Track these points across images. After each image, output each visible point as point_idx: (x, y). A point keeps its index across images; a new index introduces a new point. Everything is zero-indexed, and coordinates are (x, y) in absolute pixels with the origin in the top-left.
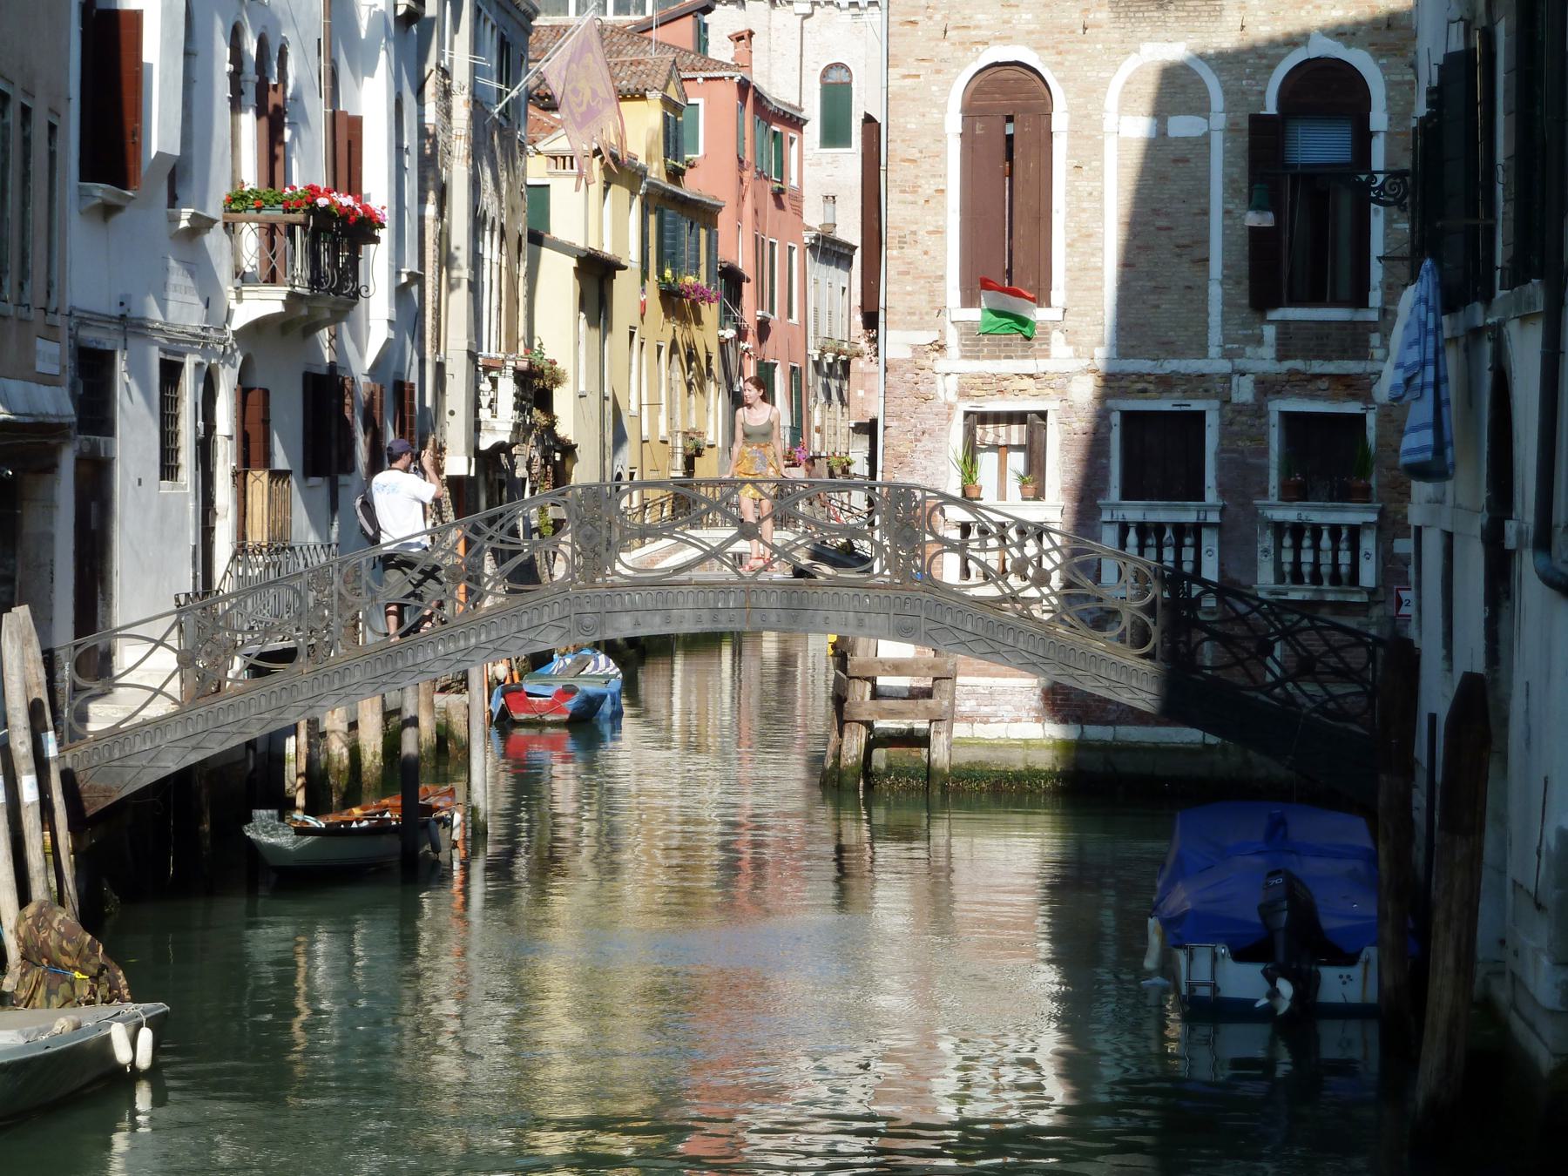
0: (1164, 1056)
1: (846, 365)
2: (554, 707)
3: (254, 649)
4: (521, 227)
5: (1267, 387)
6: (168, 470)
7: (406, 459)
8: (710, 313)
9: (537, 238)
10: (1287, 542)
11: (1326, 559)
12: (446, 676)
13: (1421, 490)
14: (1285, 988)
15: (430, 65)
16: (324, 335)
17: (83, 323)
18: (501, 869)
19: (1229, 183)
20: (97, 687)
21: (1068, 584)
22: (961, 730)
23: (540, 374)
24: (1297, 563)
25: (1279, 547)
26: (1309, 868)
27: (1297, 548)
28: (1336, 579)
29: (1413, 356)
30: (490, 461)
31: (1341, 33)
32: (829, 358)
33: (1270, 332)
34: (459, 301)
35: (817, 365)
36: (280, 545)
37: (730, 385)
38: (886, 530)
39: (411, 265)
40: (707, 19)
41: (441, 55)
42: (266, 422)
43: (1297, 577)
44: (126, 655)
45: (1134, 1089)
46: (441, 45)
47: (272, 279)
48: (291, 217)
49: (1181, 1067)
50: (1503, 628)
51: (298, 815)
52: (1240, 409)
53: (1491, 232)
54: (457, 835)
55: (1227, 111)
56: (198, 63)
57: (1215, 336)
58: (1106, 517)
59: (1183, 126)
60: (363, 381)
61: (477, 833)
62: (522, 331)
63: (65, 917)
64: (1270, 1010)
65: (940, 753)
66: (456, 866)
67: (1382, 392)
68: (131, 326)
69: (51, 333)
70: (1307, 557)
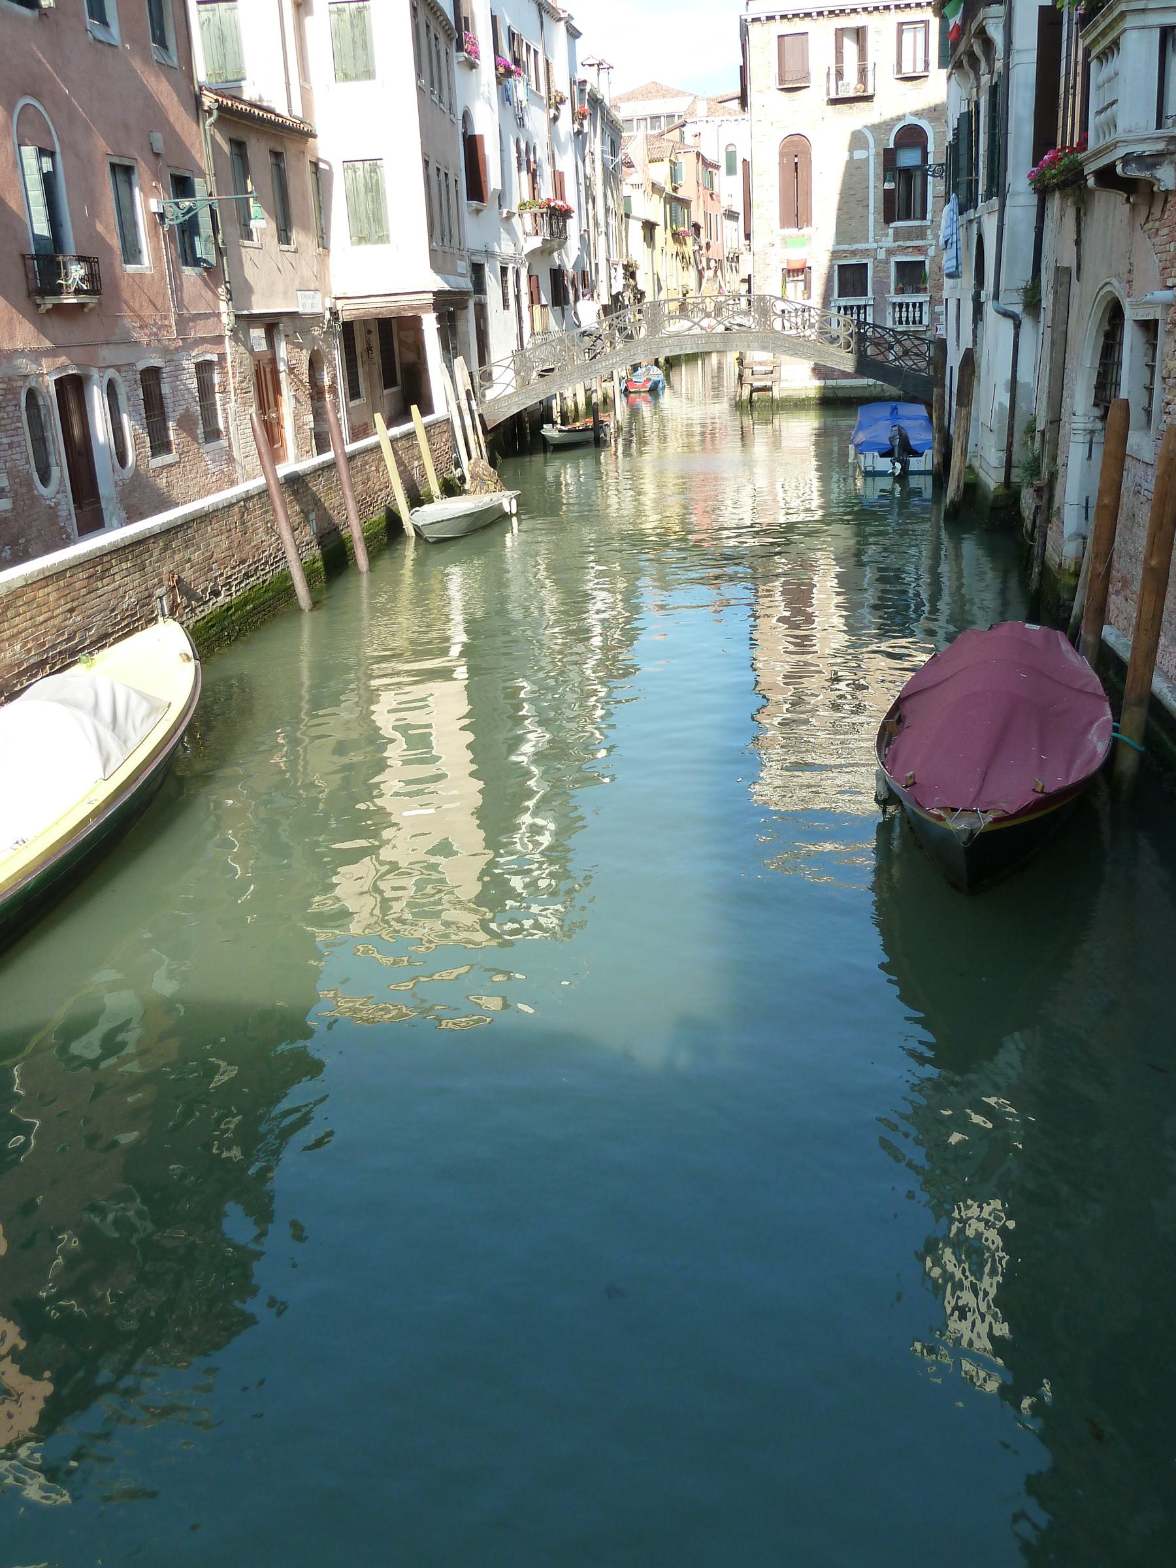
0: (855, 490)
1: (738, 257)
2: (644, 386)
3: (540, 369)
4: (622, 212)
5: (890, 252)
6: (506, 306)
7: (588, 296)
8: (689, 240)
9: (627, 216)
10: (897, 309)
11: (910, 315)
12: (606, 375)
13: (948, 283)
14: (898, 465)
15: (587, 151)
16: (556, 254)
17: (472, 254)
18: (628, 444)
19: (876, 175)
20: (488, 384)
21: (820, 328)
22: (783, 385)
23: (631, 266)
24: (901, 317)
25: (894, 311)
26: (905, 424)
27: (901, 311)
28: (914, 322)
29: (949, 231)
30: (616, 298)
31: (917, 114)
32: (731, 255)
33: (891, 231)
34: (602, 238)
35: (727, 258)
36: (546, 332)
37: (697, 267)
38: (755, 311)
39: (584, 227)
40: (683, 129)
41: (590, 147)
42: (538, 287)
43: (901, 322)
44: (496, 372)
45: (845, 504)
46: (590, 143)
47: (537, 234)
48: (542, 211)
49: (862, 492)
50: (979, 332)
51: (559, 426)
52: (880, 261)
53: (977, 181)
54: (612, 430)
55: (875, 147)
56: (505, 153)
57: (871, 234)
58: (833, 304)
59: (859, 154)
60: (570, 270)
61: (619, 429)
62: (625, 251)
63: (484, 462)
64: (893, 474)
65: (776, 394)
66: (612, 441)
67: (932, 251)
68: (489, 254)
69: (462, 258)
70: (904, 315)
